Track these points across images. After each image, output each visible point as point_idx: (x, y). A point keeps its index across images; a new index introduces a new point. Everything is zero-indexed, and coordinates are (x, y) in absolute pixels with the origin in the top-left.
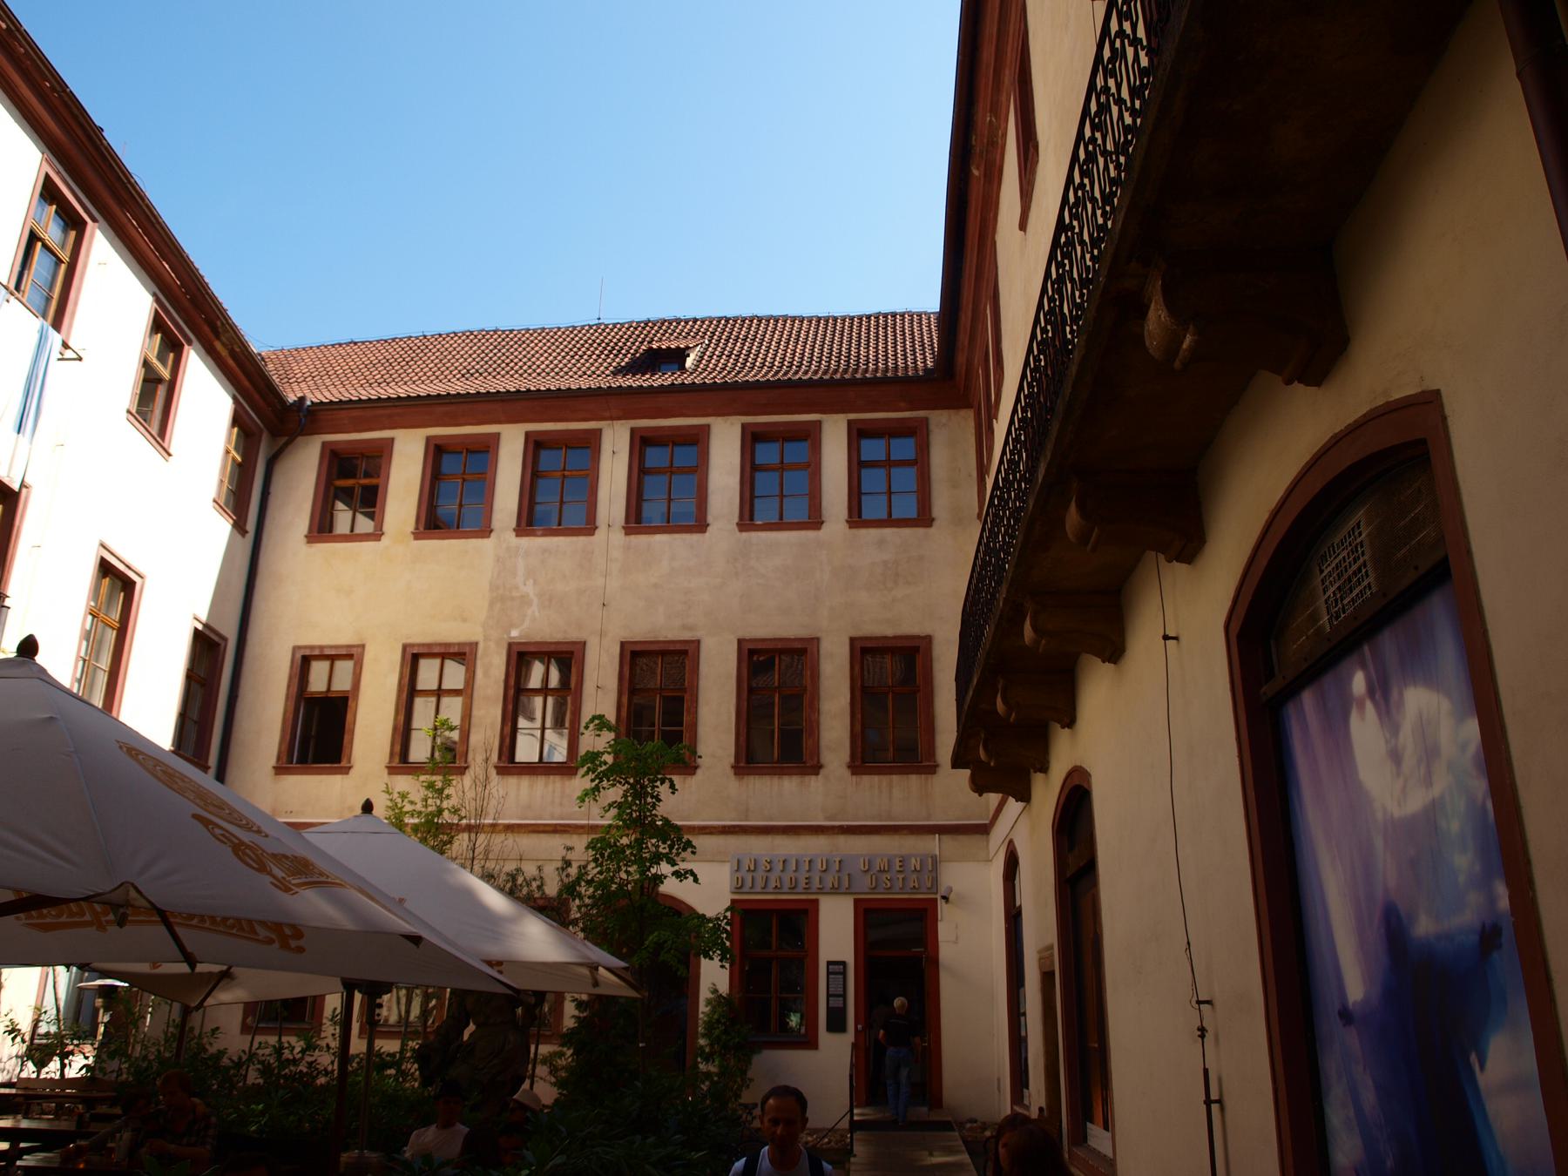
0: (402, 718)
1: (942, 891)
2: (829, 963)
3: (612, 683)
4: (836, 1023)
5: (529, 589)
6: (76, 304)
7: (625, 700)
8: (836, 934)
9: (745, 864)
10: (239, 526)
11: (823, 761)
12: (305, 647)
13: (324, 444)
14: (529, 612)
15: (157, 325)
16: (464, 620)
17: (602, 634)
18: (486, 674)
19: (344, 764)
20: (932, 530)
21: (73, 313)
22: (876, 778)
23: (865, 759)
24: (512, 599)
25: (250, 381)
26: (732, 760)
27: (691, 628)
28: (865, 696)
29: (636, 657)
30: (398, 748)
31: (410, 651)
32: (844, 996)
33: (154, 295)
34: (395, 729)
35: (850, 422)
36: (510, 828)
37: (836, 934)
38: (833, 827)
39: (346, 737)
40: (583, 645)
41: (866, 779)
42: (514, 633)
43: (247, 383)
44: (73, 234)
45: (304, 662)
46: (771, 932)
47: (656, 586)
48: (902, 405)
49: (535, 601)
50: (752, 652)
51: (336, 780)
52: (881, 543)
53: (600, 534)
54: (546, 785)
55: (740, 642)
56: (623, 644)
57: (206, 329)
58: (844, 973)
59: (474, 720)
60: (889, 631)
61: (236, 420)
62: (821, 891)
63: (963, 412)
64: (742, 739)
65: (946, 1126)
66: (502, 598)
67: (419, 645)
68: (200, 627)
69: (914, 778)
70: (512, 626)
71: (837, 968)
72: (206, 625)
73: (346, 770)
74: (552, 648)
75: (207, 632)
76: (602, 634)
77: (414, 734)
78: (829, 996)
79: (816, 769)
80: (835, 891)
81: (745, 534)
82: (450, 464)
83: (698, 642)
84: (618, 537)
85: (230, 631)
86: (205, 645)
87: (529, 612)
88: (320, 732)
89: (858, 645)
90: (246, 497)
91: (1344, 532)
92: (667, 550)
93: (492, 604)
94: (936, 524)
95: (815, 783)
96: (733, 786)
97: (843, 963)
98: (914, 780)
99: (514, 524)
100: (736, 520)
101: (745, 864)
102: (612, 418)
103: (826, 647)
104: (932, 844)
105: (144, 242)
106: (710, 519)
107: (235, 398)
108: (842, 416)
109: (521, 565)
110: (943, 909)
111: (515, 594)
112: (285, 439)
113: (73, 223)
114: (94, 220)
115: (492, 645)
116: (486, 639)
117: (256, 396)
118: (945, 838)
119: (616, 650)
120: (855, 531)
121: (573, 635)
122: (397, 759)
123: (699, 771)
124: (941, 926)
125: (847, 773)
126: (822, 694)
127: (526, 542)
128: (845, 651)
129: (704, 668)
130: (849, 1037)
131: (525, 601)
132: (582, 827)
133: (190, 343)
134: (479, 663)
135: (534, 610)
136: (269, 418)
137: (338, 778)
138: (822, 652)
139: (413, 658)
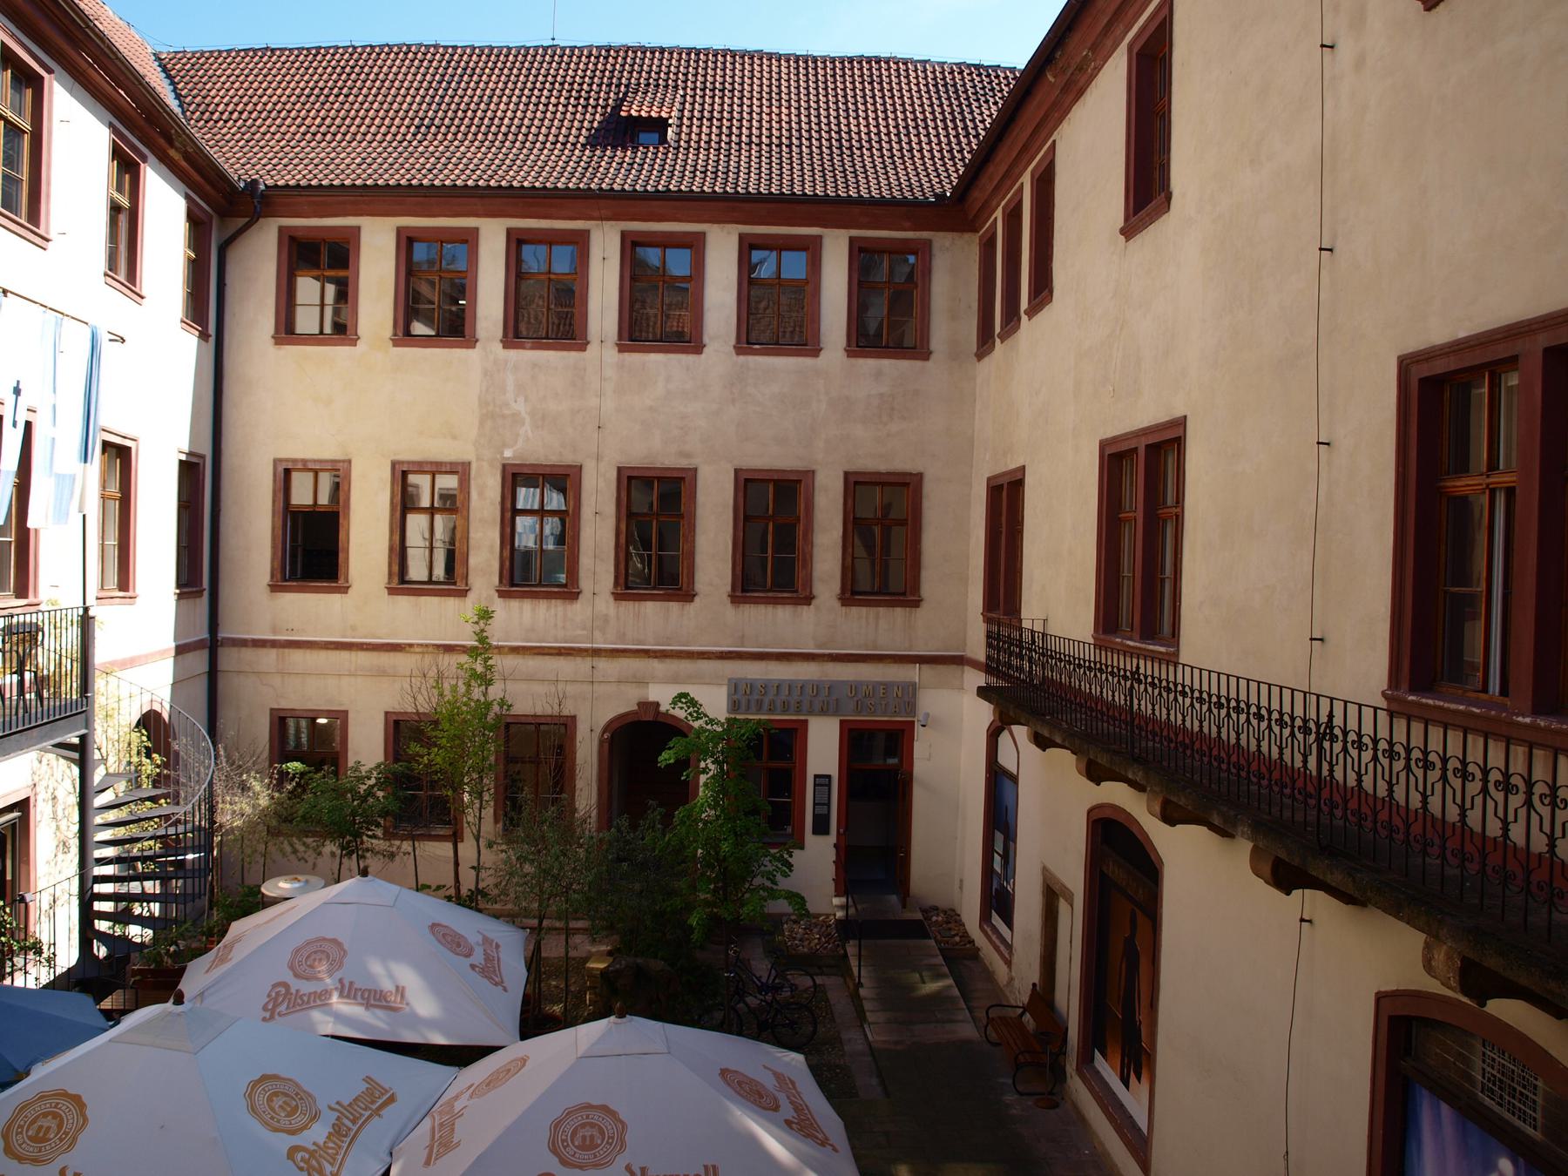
0: (397, 538)
1: (920, 716)
2: (816, 776)
3: (610, 509)
4: (821, 827)
5: (520, 407)
6: (49, 184)
7: (623, 527)
8: (823, 750)
9: (742, 688)
10: (203, 336)
11: (815, 592)
12: (287, 460)
13: (281, 229)
14: (522, 432)
15: (116, 152)
16: (454, 437)
17: (598, 458)
18: (481, 494)
19: (341, 582)
20: (929, 364)
21: (48, 196)
22: (864, 610)
23: (851, 594)
24: (503, 417)
25: (203, 176)
26: (729, 588)
27: (687, 455)
28: (855, 525)
29: (632, 482)
30: (396, 569)
31: (399, 468)
32: (829, 805)
33: (111, 125)
34: (391, 549)
35: (852, 240)
36: (515, 650)
37: (823, 750)
38: (823, 656)
39: (341, 556)
40: (579, 469)
41: (854, 610)
42: (508, 453)
43: (198, 178)
44: (29, 92)
45: (284, 476)
46: (767, 749)
47: (651, 408)
48: (907, 224)
49: (528, 420)
50: (850, 730)
51: (335, 598)
52: (878, 375)
53: (593, 349)
54: (548, 609)
55: (737, 471)
56: (620, 470)
57: (162, 141)
58: (829, 785)
59: (472, 542)
60: (883, 467)
61: (191, 217)
62: (811, 713)
63: (967, 236)
64: (739, 568)
65: (917, 930)
66: (492, 416)
67: (409, 463)
68: (183, 457)
69: (899, 610)
70: (505, 445)
71: (823, 781)
72: (189, 454)
73: (345, 590)
74: (548, 471)
75: (194, 460)
76: (598, 458)
77: (410, 552)
78: (815, 804)
79: (808, 600)
80: (824, 712)
81: (742, 358)
82: (420, 252)
83: (695, 470)
84: (611, 354)
85: (206, 449)
86: (189, 470)
87: (522, 432)
88: (312, 549)
89: (852, 479)
90: (207, 303)
91: (1507, 1116)
92: (662, 368)
93: (482, 423)
94: (933, 357)
95: (806, 613)
96: (731, 614)
97: (829, 777)
98: (899, 612)
99: (500, 333)
100: (733, 341)
101: (742, 688)
102: (602, 219)
103: (821, 479)
104: (912, 673)
105: (100, 77)
106: (706, 339)
107: (187, 197)
108: (843, 231)
109: (510, 381)
110: (919, 731)
111: (507, 412)
112: (242, 221)
113: (28, 81)
114: (50, 71)
115: (485, 464)
116: (479, 459)
117: (208, 188)
118: (924, 667)
119: (613, 475)
120: (853, 360)
121: (568, 458)
122: (396, 580)
123: (697, 599)
124: (916, 744)
125: (837, 604)
126: (816, 527)
127: (513, 354)
128: (838, 485)
129: (701, 497)
130: (832, 838)
131: (516, 419)
132: (586, 650)
133: (145, 160)
134: (472, 482)
135: (526, 429)
136: (221, 211)
137: (337, 596)
138: (817, 484)
139: (402, 475)
